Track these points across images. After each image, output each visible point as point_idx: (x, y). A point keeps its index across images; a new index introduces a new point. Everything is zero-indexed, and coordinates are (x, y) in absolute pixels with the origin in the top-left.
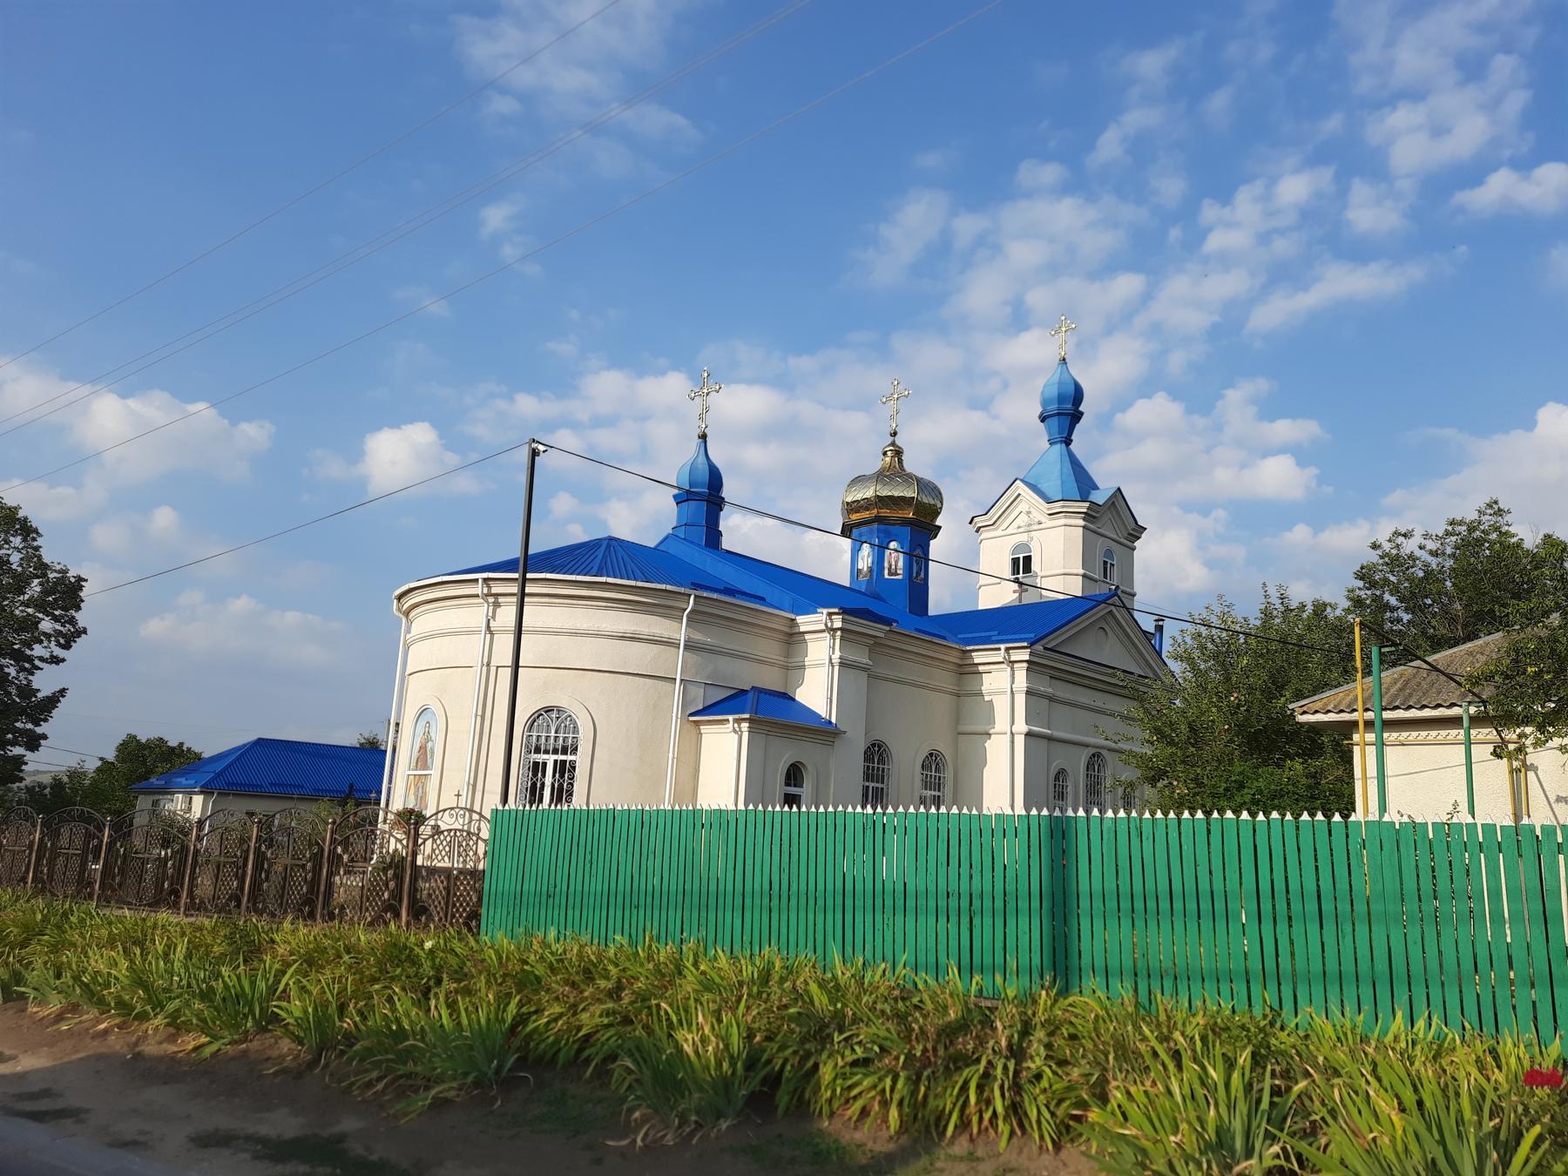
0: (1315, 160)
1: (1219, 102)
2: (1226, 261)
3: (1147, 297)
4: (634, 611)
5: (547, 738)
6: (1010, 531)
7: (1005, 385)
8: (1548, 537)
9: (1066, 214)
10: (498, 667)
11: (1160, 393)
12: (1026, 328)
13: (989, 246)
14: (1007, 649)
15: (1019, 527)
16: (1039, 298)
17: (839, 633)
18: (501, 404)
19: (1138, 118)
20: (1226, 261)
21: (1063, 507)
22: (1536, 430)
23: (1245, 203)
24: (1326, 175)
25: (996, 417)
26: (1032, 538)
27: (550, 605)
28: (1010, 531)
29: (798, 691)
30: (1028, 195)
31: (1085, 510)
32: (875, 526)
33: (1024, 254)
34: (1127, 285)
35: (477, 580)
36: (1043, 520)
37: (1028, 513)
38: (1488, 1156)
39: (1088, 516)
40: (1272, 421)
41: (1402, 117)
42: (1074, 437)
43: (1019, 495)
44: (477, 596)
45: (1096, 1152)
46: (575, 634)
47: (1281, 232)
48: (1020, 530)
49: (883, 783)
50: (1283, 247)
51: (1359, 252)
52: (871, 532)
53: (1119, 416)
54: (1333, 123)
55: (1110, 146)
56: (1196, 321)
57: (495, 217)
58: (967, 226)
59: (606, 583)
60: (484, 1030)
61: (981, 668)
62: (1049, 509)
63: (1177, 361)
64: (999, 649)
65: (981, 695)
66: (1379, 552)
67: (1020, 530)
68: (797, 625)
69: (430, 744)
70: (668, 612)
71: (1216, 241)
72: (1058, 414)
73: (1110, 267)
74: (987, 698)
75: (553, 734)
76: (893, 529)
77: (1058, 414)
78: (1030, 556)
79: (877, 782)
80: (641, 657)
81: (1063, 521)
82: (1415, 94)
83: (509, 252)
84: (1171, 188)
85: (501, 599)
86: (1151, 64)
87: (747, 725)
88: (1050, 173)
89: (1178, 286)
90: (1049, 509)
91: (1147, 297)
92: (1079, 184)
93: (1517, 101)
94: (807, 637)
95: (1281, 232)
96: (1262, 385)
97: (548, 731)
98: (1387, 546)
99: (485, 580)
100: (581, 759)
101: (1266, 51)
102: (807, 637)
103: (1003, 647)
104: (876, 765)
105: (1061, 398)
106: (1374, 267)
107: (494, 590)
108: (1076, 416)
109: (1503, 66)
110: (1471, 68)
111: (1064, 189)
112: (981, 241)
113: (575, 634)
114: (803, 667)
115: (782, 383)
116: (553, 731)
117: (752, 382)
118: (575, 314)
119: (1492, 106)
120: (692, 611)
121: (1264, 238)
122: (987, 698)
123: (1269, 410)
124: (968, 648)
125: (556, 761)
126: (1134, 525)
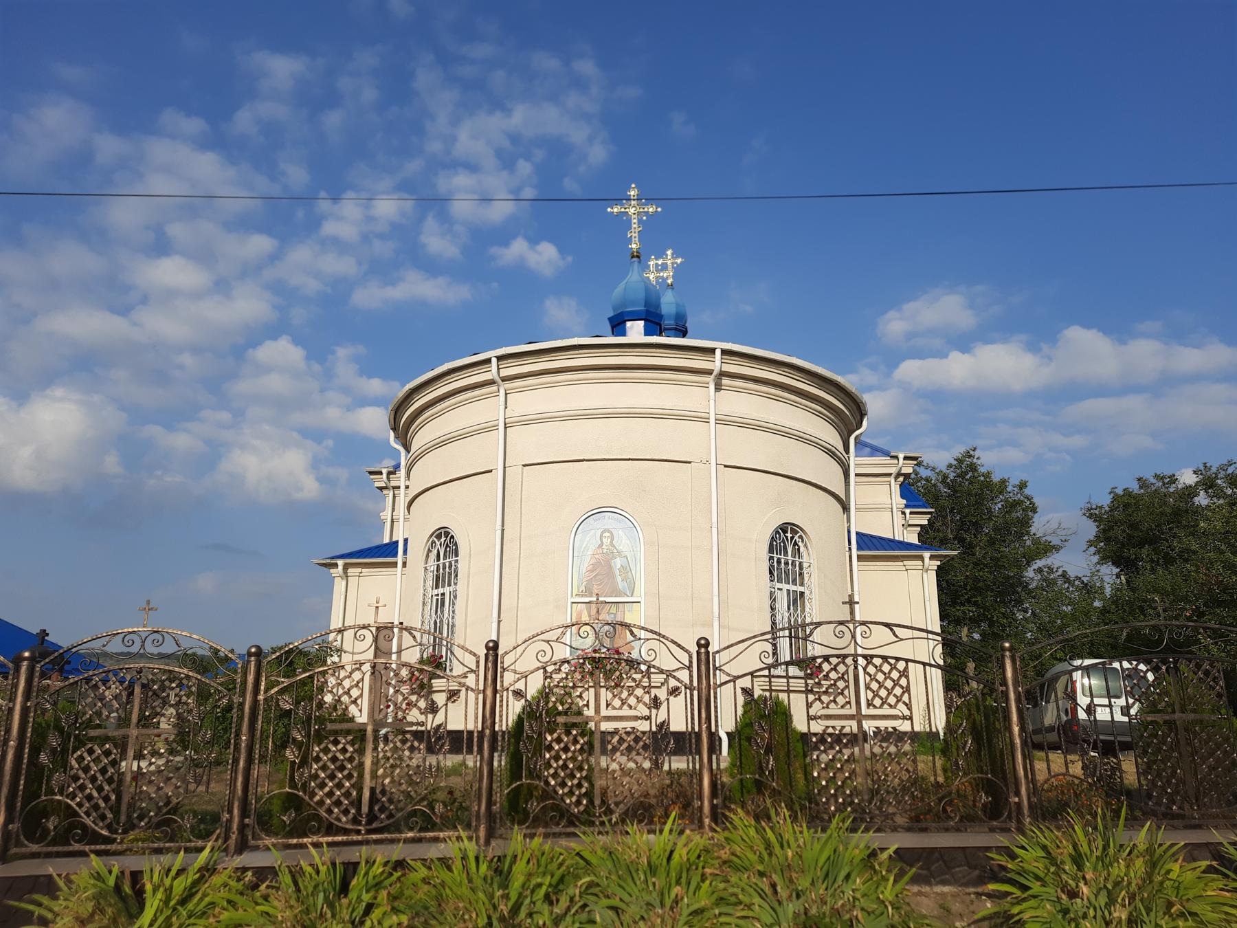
0: (405, 187)
1: (333, 120)
2: (338, 245)
3: (274, 258)
7: (144, 300)
11: (285, 337)
16: (177, 231)
20: (338, 245)
23: (350, 208)
34: (261, 244)
38: (16, 854)
40: (370, 377)
41: (462, 180)
49: (802, 585)
50: (383, 249)
51: (432, 267)
53: (251, 351)
54: (413, 167)
55: (244, 121)
58: (109, 146)
63: (299, 315)
69: (618, 563)
71: (329, 228)
72: (676, 329)
73: (244, 224)
79: (794, 582)
84: (297, 175)
88: (194, 125)
89: (301, 254)
91: (274, 258)
96: (361, 349)
104: (790, 557)
106: (441, 280)
109: (524, 168)
110: (507, 161)
121: (366, 238)
123: (368, 370)
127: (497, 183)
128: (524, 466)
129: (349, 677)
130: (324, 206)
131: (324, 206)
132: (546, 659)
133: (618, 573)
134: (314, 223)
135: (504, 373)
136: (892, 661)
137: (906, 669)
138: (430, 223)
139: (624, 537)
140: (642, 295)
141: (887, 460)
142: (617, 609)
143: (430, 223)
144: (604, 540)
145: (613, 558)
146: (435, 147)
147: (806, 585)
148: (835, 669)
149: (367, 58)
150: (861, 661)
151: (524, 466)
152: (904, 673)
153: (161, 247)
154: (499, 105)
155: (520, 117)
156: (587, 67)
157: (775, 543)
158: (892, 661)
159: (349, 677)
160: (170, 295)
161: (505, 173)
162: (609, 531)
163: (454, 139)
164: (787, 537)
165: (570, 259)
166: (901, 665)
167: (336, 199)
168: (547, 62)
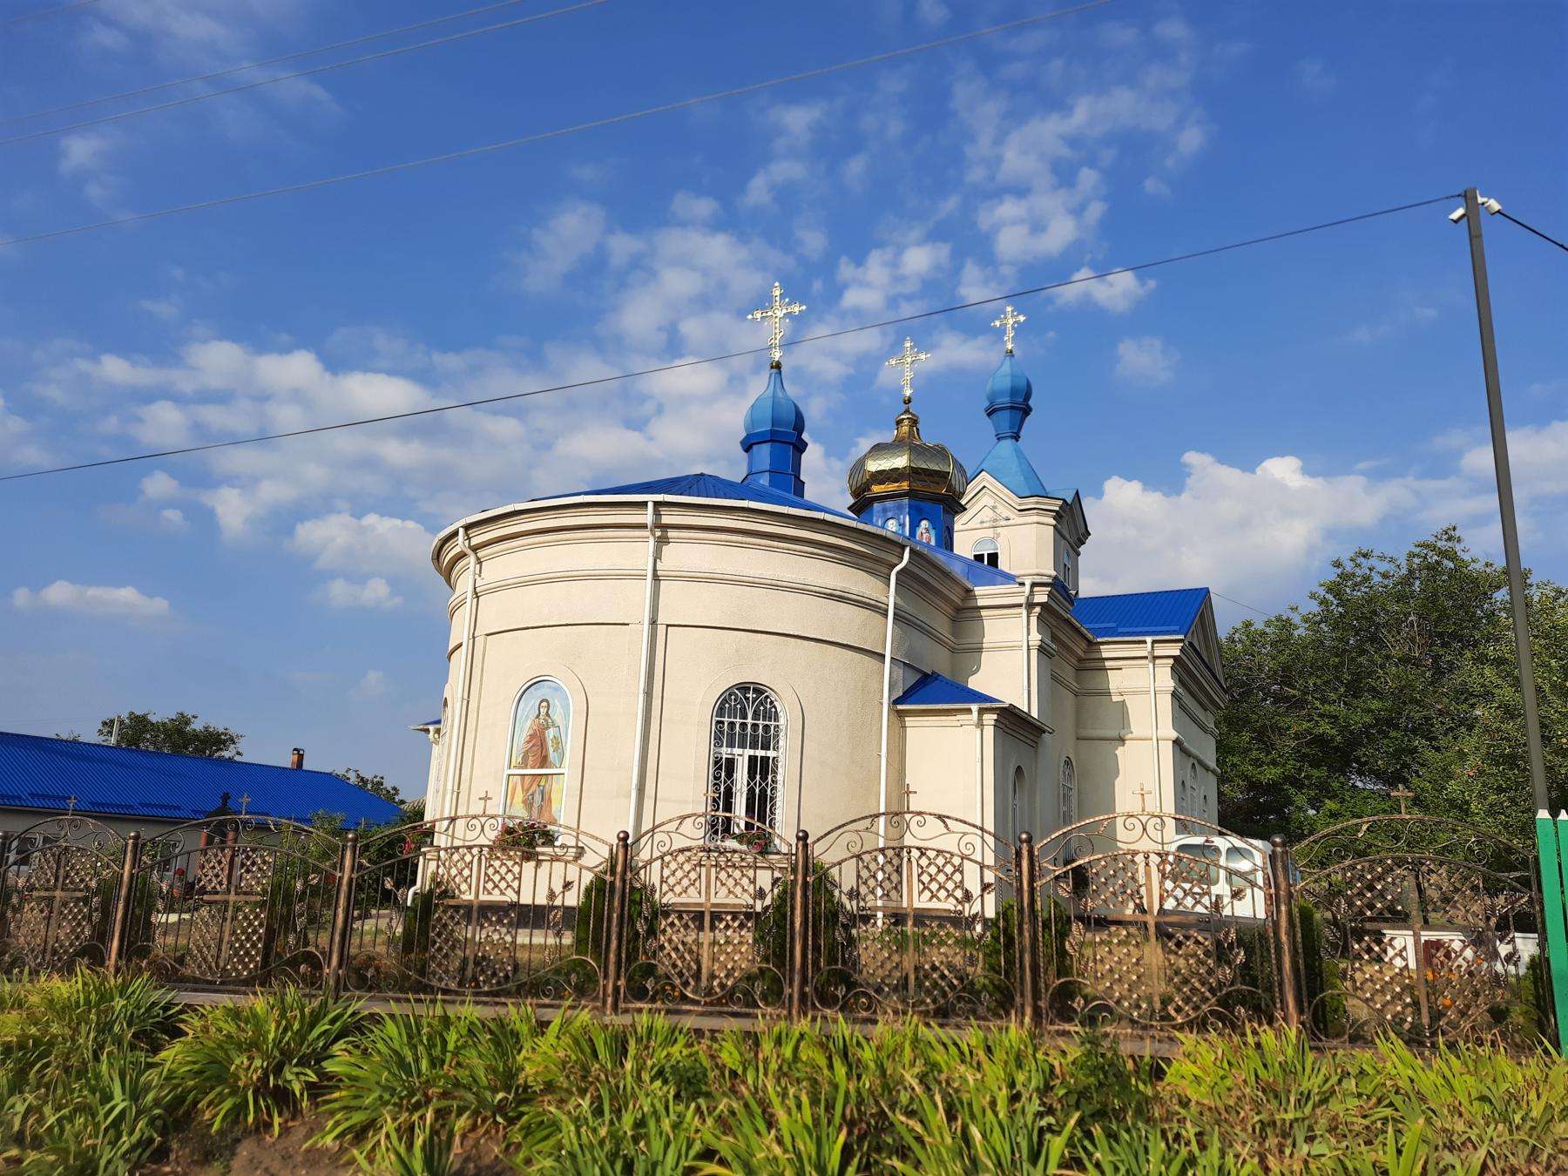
0: (935, 236)
1: (855, 168)
4: (841, 562)
5: (744, 725)
6: (971, 525)
7: (660, 410)
8: (1207, 591)
9: (718, 250)
10: (668, 626)
12: (681, 356)
13: (642, 268)
14: (1154, 642)
15: (982, 522)
16: (692, 328)
17: (1038, 609)
18: (83, 365)
19: (786, 170)
20: (861, 319)
21: (1037, 503)
22: (1105, 498)
23: (876, 269)
24: (943, 251)
25: (651, 439)
26: (999, 535)
27: (741, 545)
28: (971, 525)
29: (970, 679)
30: (683, 224)
31: (1057, 509)
32: (906, 501)
33: (677, 283)
35: (645, 504)
36: (1011, 516)
37: (994, 508)
39: (1058, 516)
41: (1008, 209)
42: (1021, 434)
43: (984, 487)
44: (644, 526)
45: (217, 1132)
46: (775, 586)
47: (910, 298)
48: (985, 525)
52: (900, 508)
54: (950, 205)
55: (758, 191)
56: (833, 370)
57: (80, 150)
58: (622, 246)
59: (824, 522)
60: (284, 1108)
61: (1108, 664)
62: (1020, 504)
64: (1145, 642)
65: (1109, 694)
66: (1339, 571)
67: (985, 525)
68: (974, 597)
69: (551, 733)
70: (876, 567)
71: (852, 298)
72: (1011, 408)
74: (1115, 699)
75: (749, 721)
76: (926, 505)
77: (1011, 408)
78: (997, 554)
80: (849, 623)
81: (1035, 518)
82: (1020, 191)
83: (94, 192)
84: (814, 241)
85: (671, 534)
86: (798, 120)
87: (995, 717)
88: (704, 207)
90: (1020, 504)
92: (729, 222)
93: (1096, 210)
94: (984, 613)
95: (910, 298)
97: (745, 717)
98: (1349, 566)
99: (657, 504)
100: (785, 755)
101: (896, 128)
102: (984, 613)
103: (1149, 639)
105: (1014, 391)
107: (666, 520)
108: (1027, 411)
109: (1088, 178)
110: (1064, 175)
111: (716, 226)
112: (636, 263)
113: (775, 586)
114: (980, 650)
115: (422, 377)
116: (750, 715)
117: (391, 373)
118: (178, 273)
119: (1078, 211)
120: (902, 570)
121: (893, 302)
122: (1115, 699)
124: (1099, 640)
125: (752, 759)
126: (1084, 530)
127: (1050, 203)
128: (488, 635)
129: (679, 883)
130: (846, 270)
131: (846, 270)
132: (665, 850)
133: (550, 743)
134: (835, 292)
135: (474, 541)
136: (948, 856)
137: (961, 865)
138: (971, 271)
139: (559, 707)
140: (769, 413)
141: (1014, 588)
142: (546, 781)
143: (971, 271)
144: (542, 710)
145: (548, 728)
146: (976, 175)
147: (781, 751)
148: (940, 871)
149: (893, 84)
150: (915, 853)
151: (488, 635)
152: (959, 869)
153: (673, 347)
154: (1057, 103)
155: (1083, 113)
156: (1174, 30)
157: (727, 705)
158: (948, 856)
159: (679, 883)
160: (685, 400)
161: (1062, 192)
162: (547, 701)
163: (1000, 159)
164: (747, 699)
165: (1152, 284)
166: (956, 861)
167: (859, 261)
168: (1122, 35)
